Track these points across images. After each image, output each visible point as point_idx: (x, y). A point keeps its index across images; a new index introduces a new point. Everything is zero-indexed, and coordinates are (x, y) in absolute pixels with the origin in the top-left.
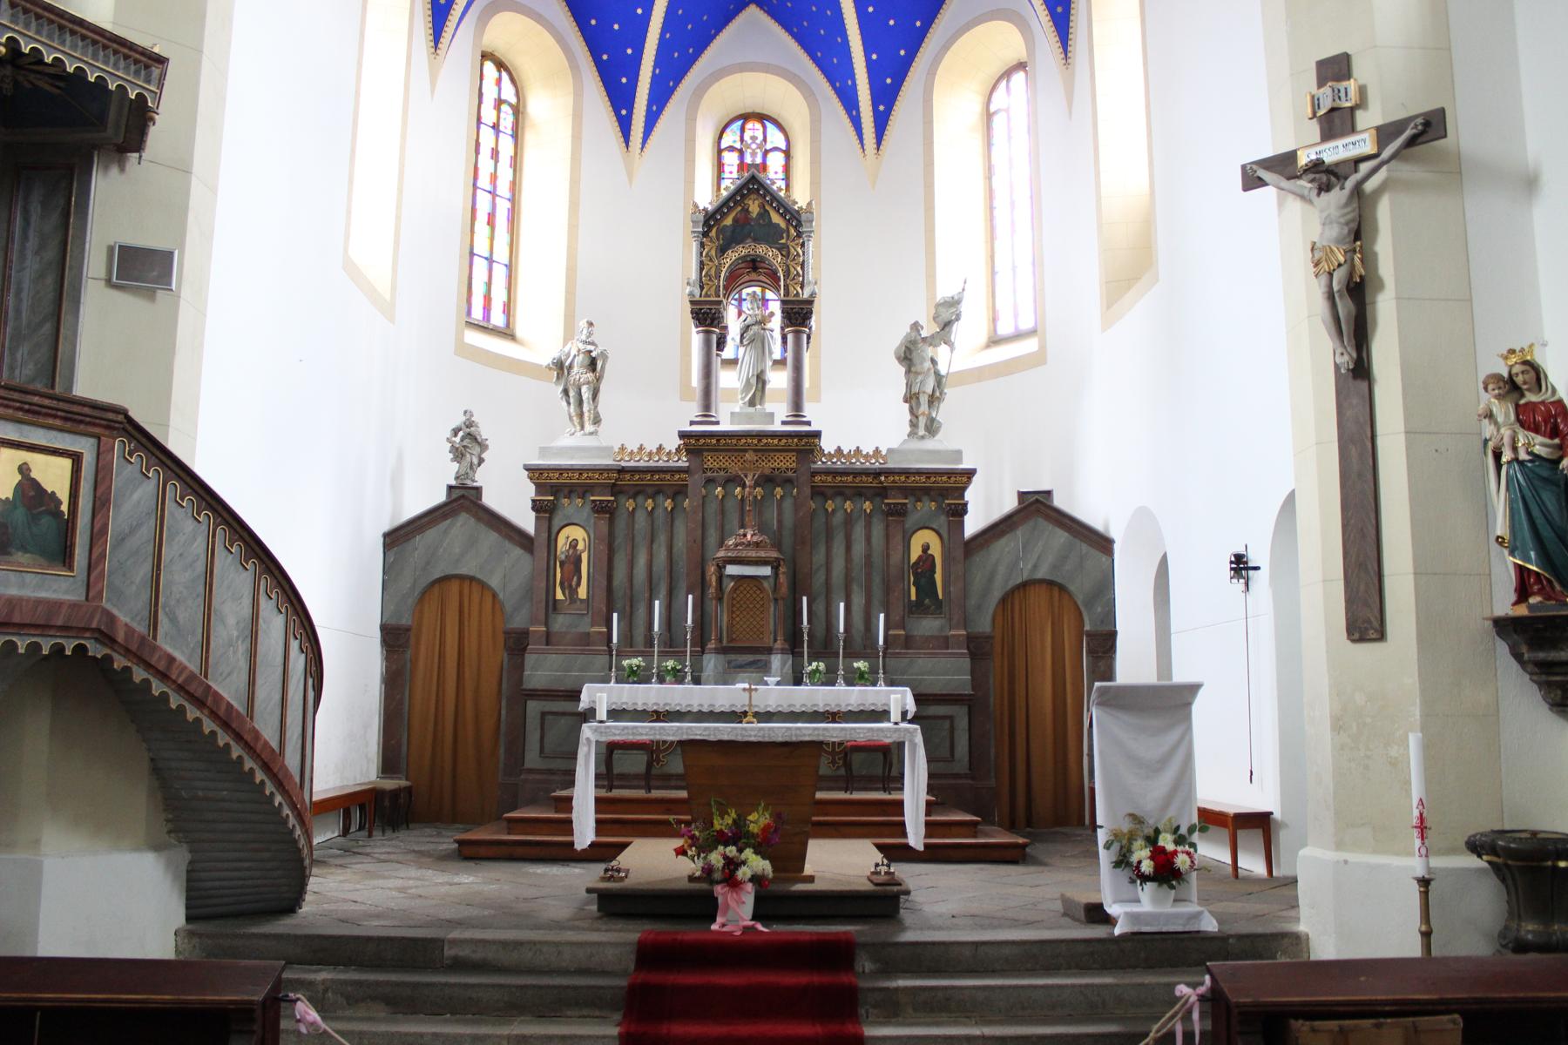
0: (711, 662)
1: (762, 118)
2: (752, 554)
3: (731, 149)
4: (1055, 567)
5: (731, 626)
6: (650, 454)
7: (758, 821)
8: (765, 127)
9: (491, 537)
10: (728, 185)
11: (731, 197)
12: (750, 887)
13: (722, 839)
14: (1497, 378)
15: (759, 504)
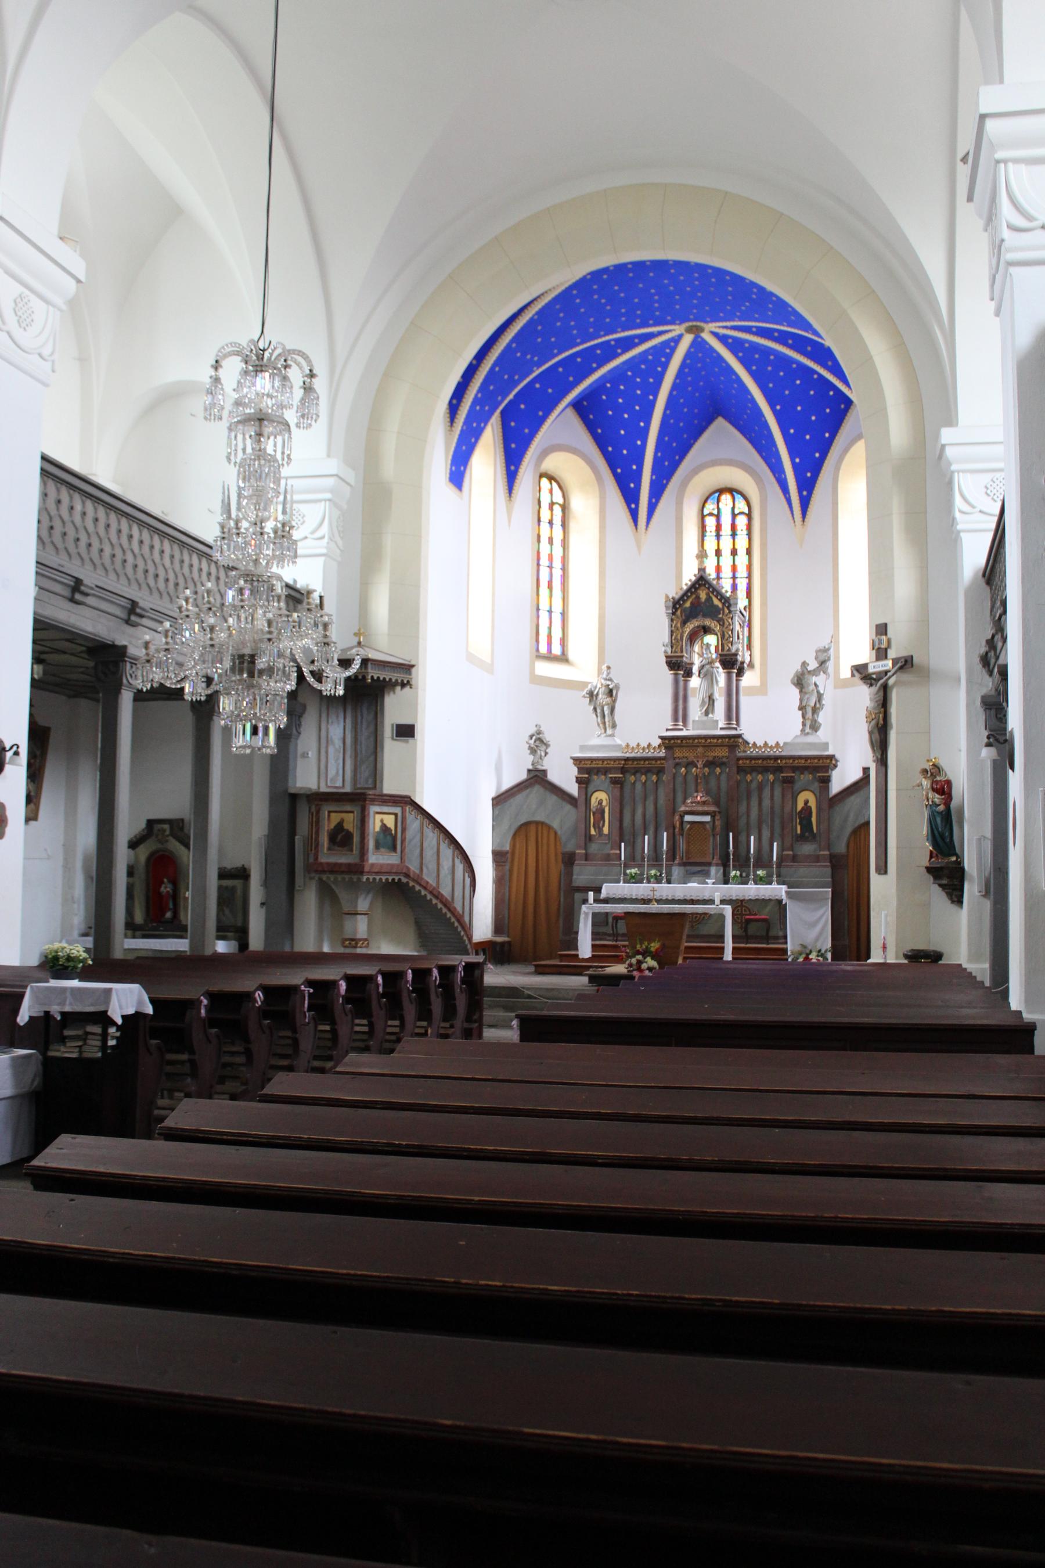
0: (676, 871)
1: (731, 491)
2: (700, 809)
5: (688, 852)
6: (644, 749)
7: (654, 946)
9: (553, 799)
11: (689, 590)
13: (638, 953)
15: (706, 778)
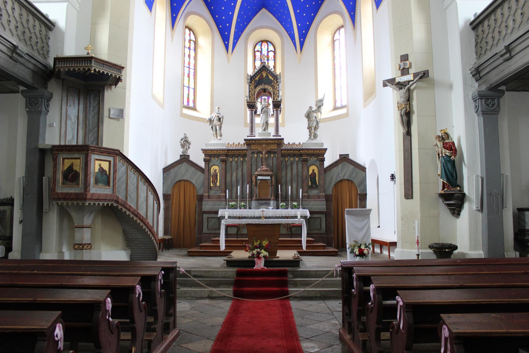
0: (254, 203)
1: (267, 41)
2: (265, 173)
3: (258, 51)
4: (350, 176)
6: (236, 145)
7: (265, 243)
8: (268, 45)
10: (258, 64)
11: (258, 72)
12: (263, 259)
13: (256, 247)
14: (439, 137)
